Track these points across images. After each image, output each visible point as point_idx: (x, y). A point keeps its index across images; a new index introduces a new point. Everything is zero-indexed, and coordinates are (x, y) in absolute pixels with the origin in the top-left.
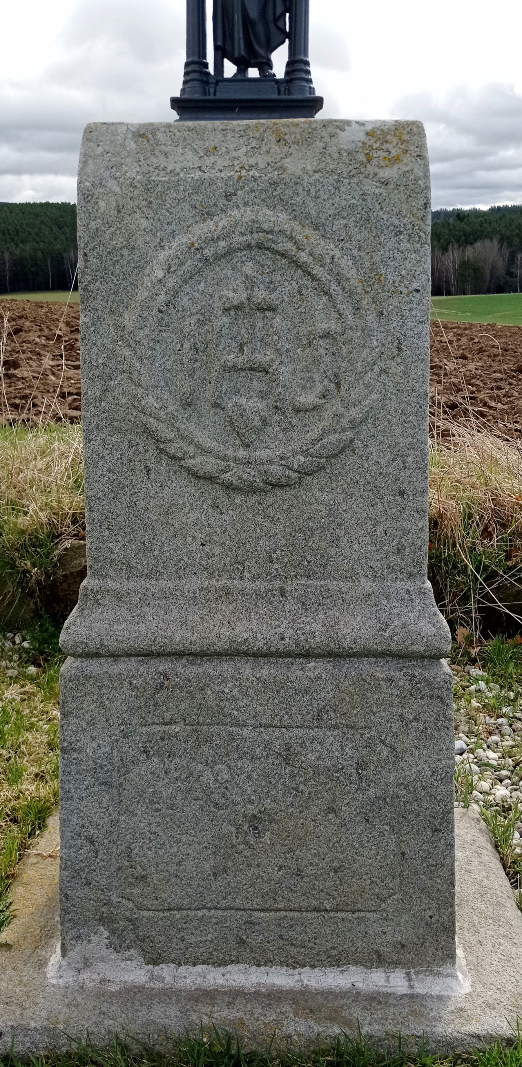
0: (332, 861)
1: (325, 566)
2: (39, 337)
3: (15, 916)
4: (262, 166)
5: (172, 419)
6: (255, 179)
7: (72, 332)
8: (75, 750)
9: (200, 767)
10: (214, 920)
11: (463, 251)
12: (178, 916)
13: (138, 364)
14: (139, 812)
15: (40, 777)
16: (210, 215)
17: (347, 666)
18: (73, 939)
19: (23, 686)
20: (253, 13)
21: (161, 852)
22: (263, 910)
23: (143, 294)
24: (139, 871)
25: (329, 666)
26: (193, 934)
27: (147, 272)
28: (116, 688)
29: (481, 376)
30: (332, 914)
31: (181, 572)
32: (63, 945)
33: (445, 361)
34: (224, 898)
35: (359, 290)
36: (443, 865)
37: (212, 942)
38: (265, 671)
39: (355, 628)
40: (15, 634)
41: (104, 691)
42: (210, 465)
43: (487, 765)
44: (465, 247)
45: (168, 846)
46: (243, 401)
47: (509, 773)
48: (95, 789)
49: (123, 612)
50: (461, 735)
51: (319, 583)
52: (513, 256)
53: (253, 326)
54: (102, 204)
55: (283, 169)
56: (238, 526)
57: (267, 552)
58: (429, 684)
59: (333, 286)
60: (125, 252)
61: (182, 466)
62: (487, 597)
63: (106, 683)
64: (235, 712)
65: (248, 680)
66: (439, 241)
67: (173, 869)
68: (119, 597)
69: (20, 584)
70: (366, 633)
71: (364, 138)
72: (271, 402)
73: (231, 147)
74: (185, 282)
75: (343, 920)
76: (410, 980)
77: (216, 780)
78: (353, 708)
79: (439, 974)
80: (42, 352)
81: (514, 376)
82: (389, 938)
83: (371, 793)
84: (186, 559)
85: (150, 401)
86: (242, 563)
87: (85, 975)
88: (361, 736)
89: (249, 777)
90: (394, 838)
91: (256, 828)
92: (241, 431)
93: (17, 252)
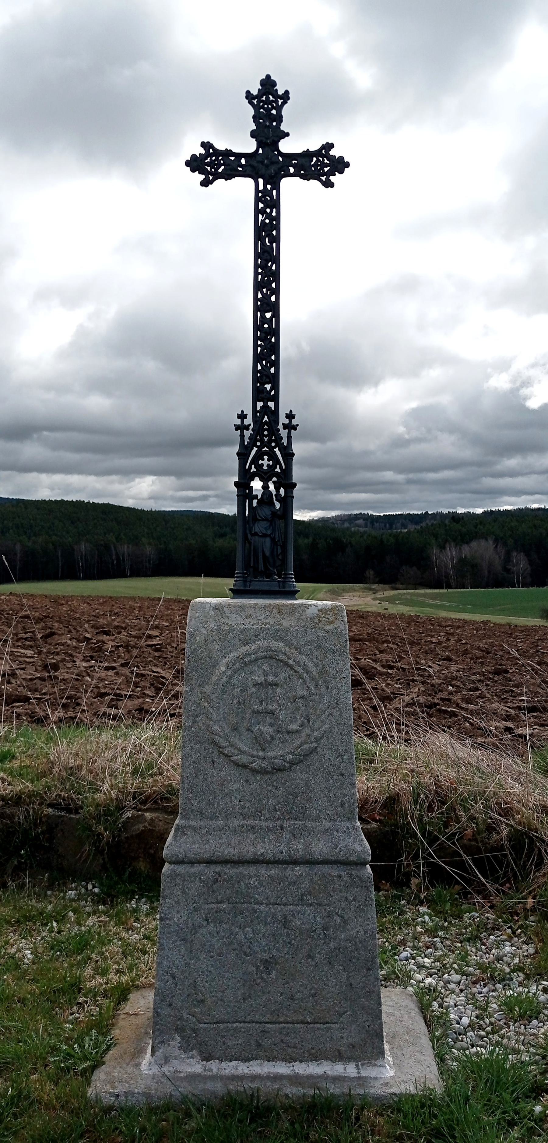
0: (311, 990)
1: (304, 814)
2: (70, 639)
3: (117, 1043)
4: (271, 623)
5: (226, 738)
6: (268, 629)
7: (97, 633)
8: (167, 919)
9: (237, 930)
10: (243, 1030)
11: (460, 549)
12: (222, 1027)
13: (211, 710)
14: (202, 958)
15: (118, 971)
16: (248, 643)
17: (317, 868)
18: (158, 1043)
19: (99, 917)
20: (268, 554)
21: (213, 984)
22: (272, 1023)
23: (214, 678)
24: (200, 997)
25: (307, 869)
26: (230, 1039)
27: (217, 668)
28: (192, 882)
29: (461, 677)
30: (312, 1025)
31: (229, 817)
32: (153, 1047)
33: (430, 663)
34: (249, 1015)
35: (317, 677)
36: (374, 992)
37: (241, 1045)
38: (273, 872)
39: (320, 848)
40: (87, 884)
41: (186, 883)
42: (245, 759)
43: (423, 966)
44: (461, 545)
45: (217, 980)
46: (262, 728)
47: (436, 971)
48: (178, 943)
49: (197, 838)
50: (408, 948)
51: (301, 823)
52: (508, 554)
53: (267, 693)
54: (198, 638)
55: (281, 625)
56: (259, 791)
57: (274, 806)
58: (360, 878)
59: (305, 675)
60: (208, 659)
61: (230, 760)
62: (429, 854)
63: (187, 878)
64: (257, 896)
65: (263, 876)
66: (436, 540)
67: (220, 995)
68: (195, 829)
69: (94, 844)
70: (326, 850)
71: (317, 612)
72: (276, 728)
73: (258, 615)
74: (235, 673)
75: (318, 1029)
76: (358, 1069)
77: (246, 938)
78: (320, 893)
79: (375, 1065)
80: (74, 654)
81: (490, 678)
82: (345, 1041)
83: (332, 945)
84: (231, 809)
85: (216, 728)
86: (260, 812)
87: (165, 1069)
88: (325, 910)
89: (264, 935)
90: (345, 974)
91: (268, 968)
92: (261, 742)
93: (30, 544)
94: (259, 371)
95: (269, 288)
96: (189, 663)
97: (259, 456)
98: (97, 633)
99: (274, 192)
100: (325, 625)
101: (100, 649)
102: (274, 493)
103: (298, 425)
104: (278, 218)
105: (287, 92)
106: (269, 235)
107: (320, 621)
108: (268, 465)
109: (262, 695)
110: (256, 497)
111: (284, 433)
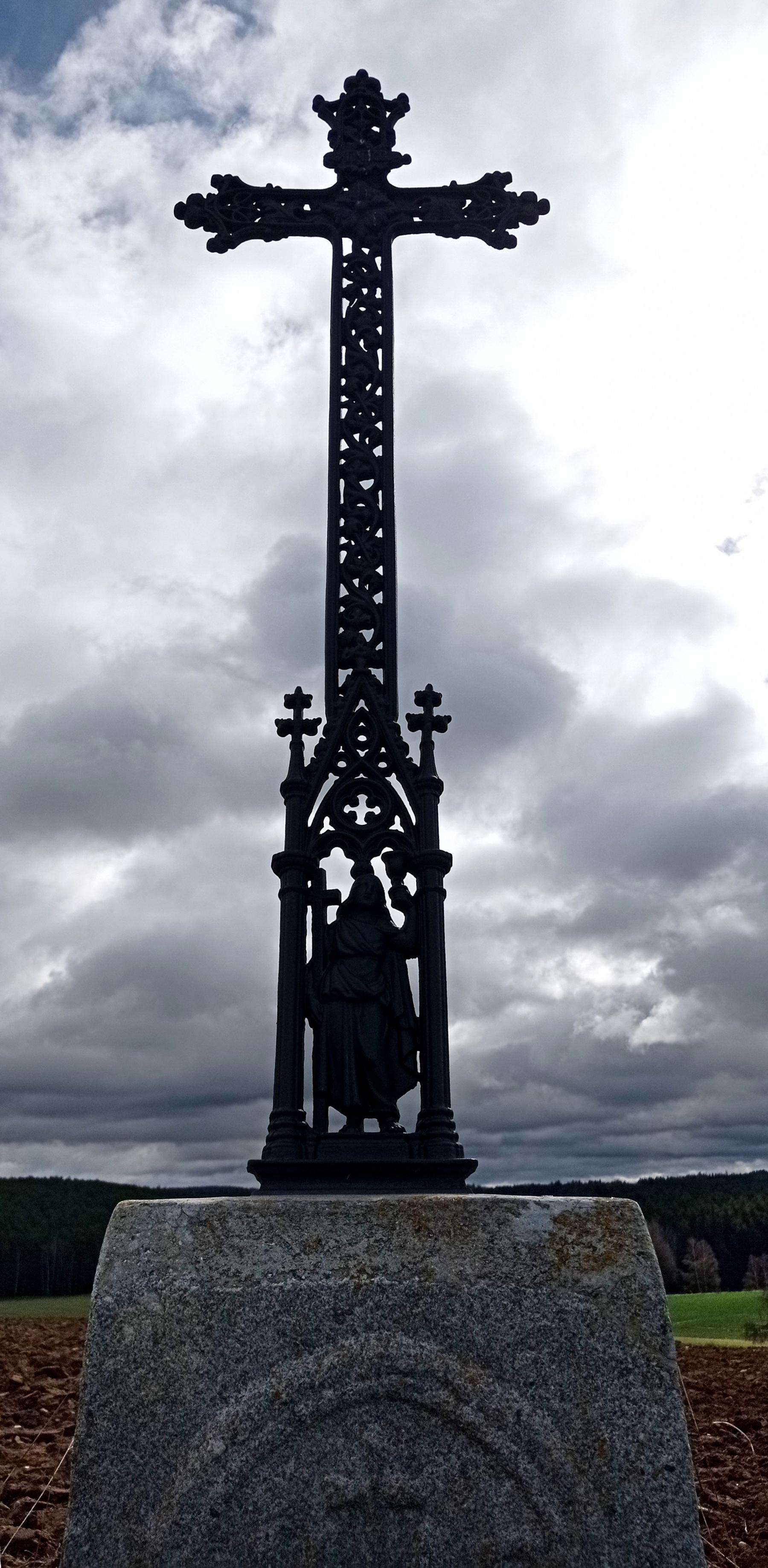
16: (309, 1346)
23: (184, 1484)
27: (194, 1442)
35: (569, 1468)
54: (129, 1330)
55: (427, 1273)
59: (524, 1464)
73: (344, 1239)
74: (262, 1459)
94: (344, 601)
95: (367, 430)
96: (90, 1424)
97: (345, 793)
98: (37, 1374)
99: (378, 260)
100: (585, 1271)
101: (34, 1403)
102: (387, 884)
103: (449, 719)
104: (387, 302)
105: (403, 98)
106: (367, 333)
107: (564, 1259)
108: (369, 817)
109: (364, 1548)
110: (335, 896)
111: (413, 740)
